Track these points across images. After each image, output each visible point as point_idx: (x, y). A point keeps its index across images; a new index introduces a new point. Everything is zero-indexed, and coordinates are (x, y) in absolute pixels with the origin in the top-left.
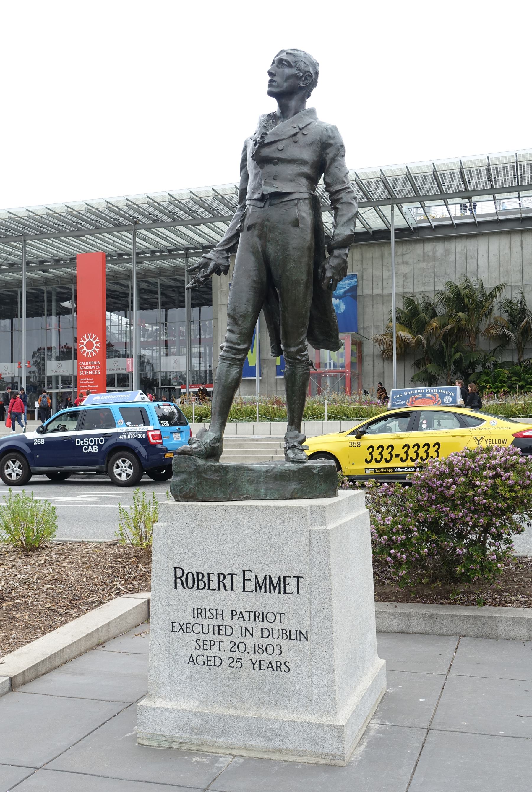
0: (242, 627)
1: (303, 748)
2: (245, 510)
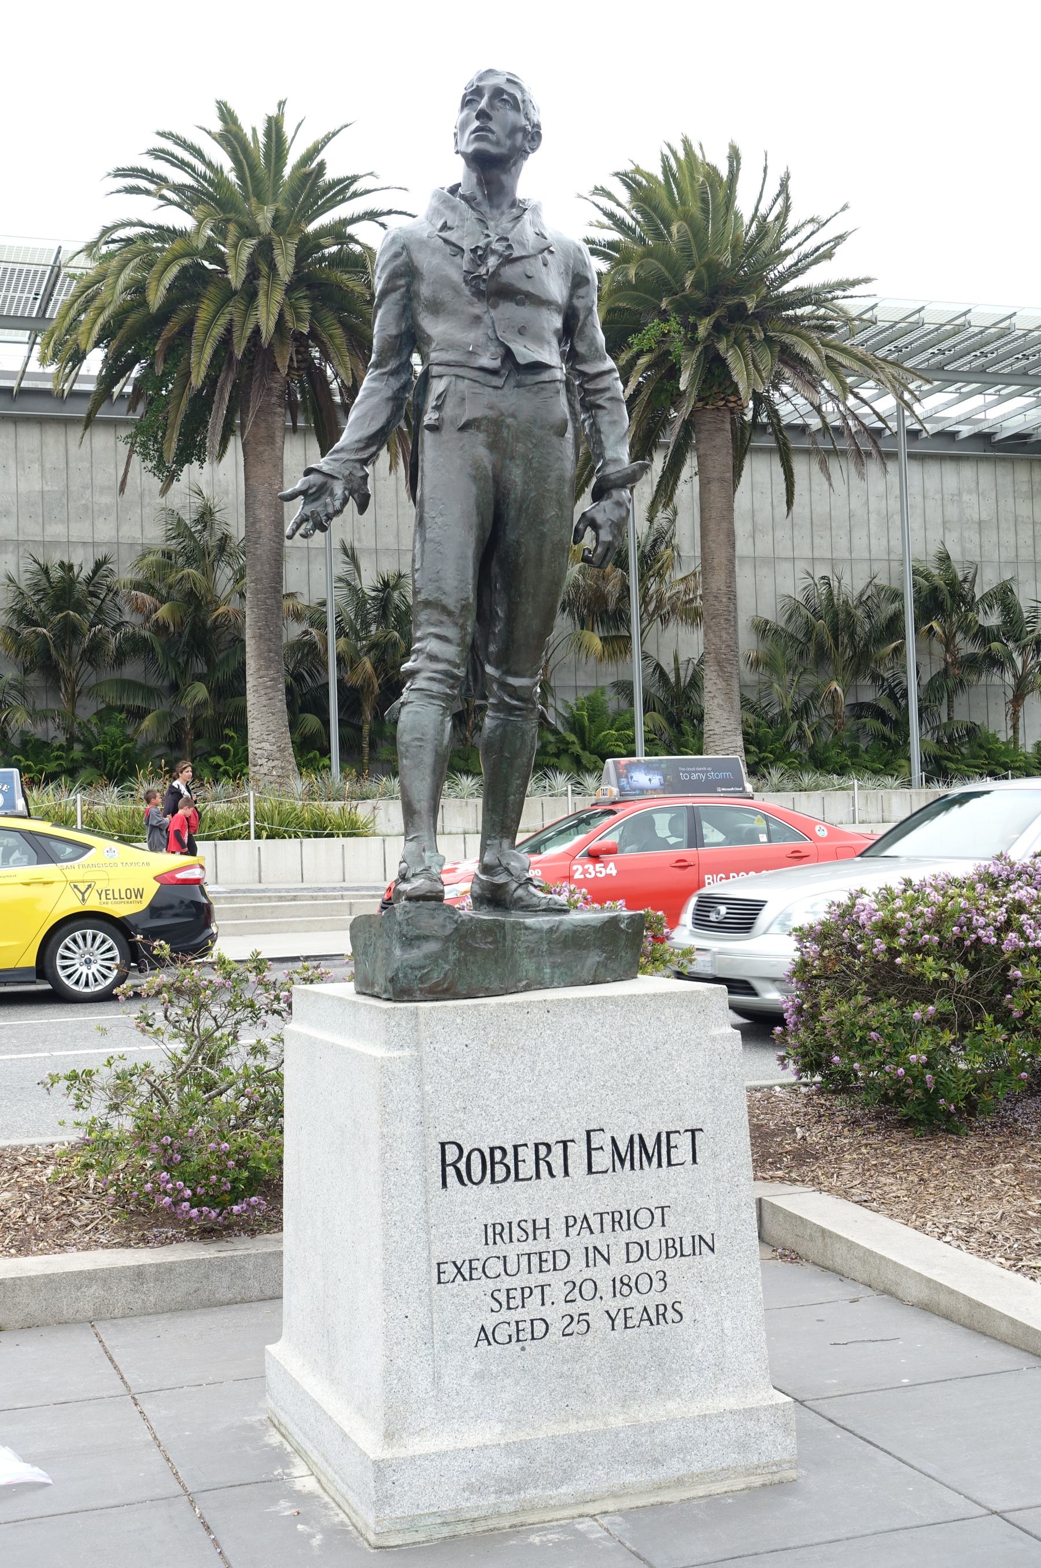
0: (587, 1249)
1: (724, 1465)
2: (588, 1007)
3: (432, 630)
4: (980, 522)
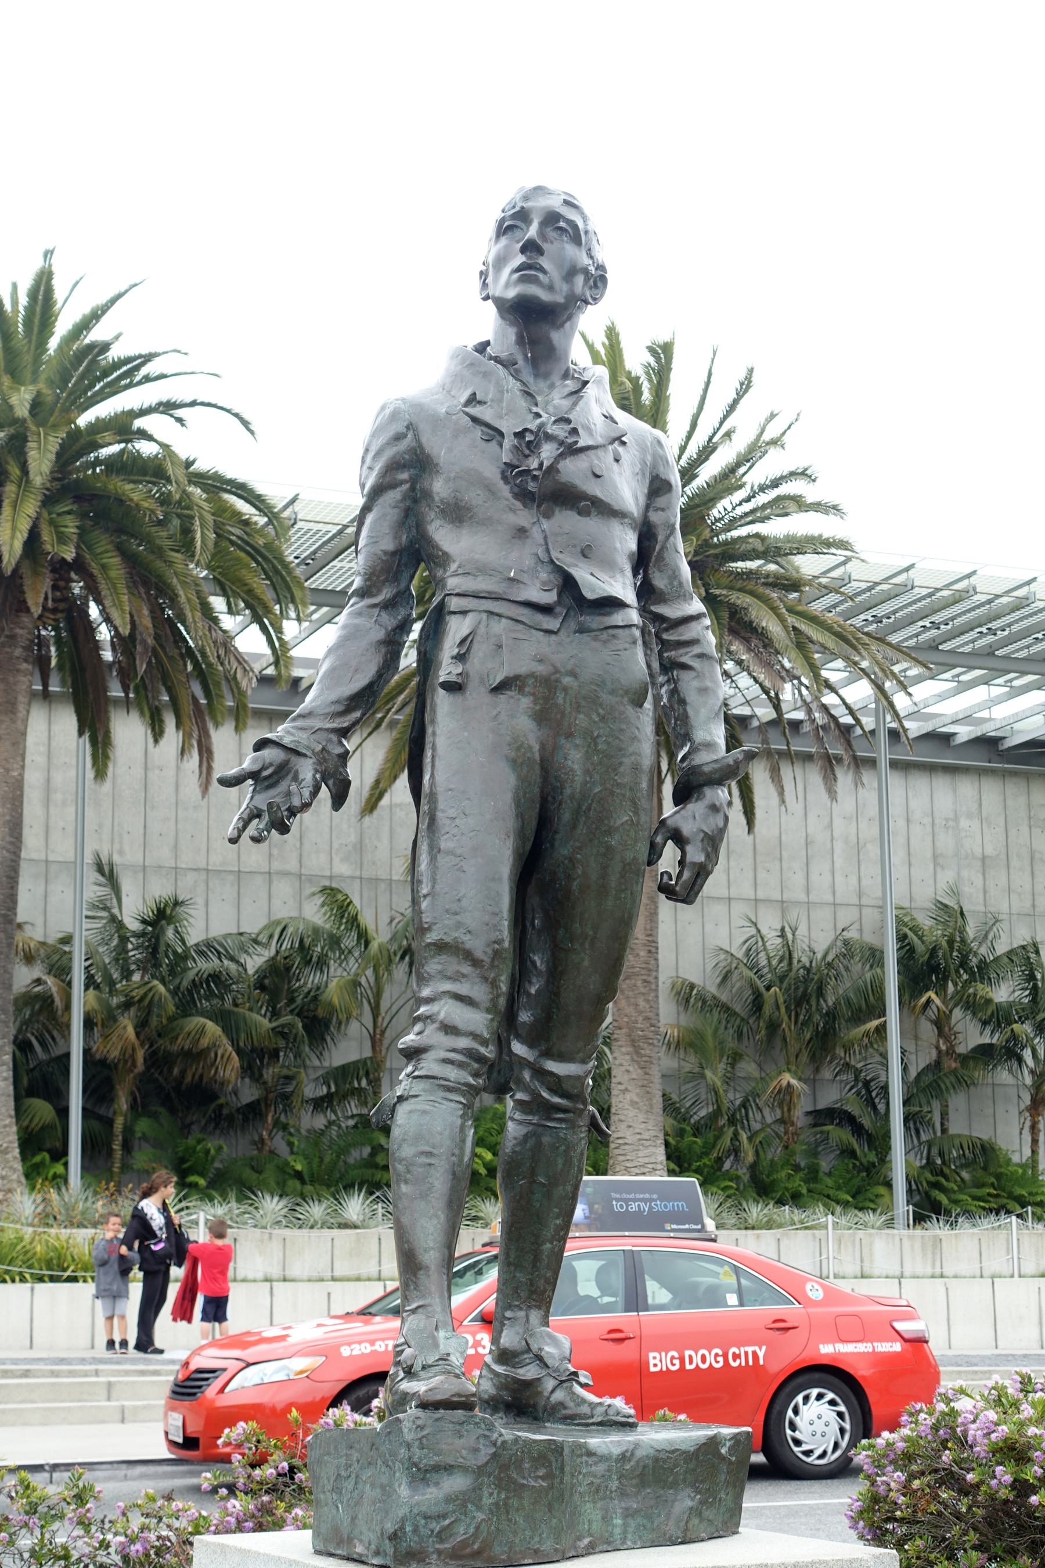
3: (448, 986)
4: (984, 859)
